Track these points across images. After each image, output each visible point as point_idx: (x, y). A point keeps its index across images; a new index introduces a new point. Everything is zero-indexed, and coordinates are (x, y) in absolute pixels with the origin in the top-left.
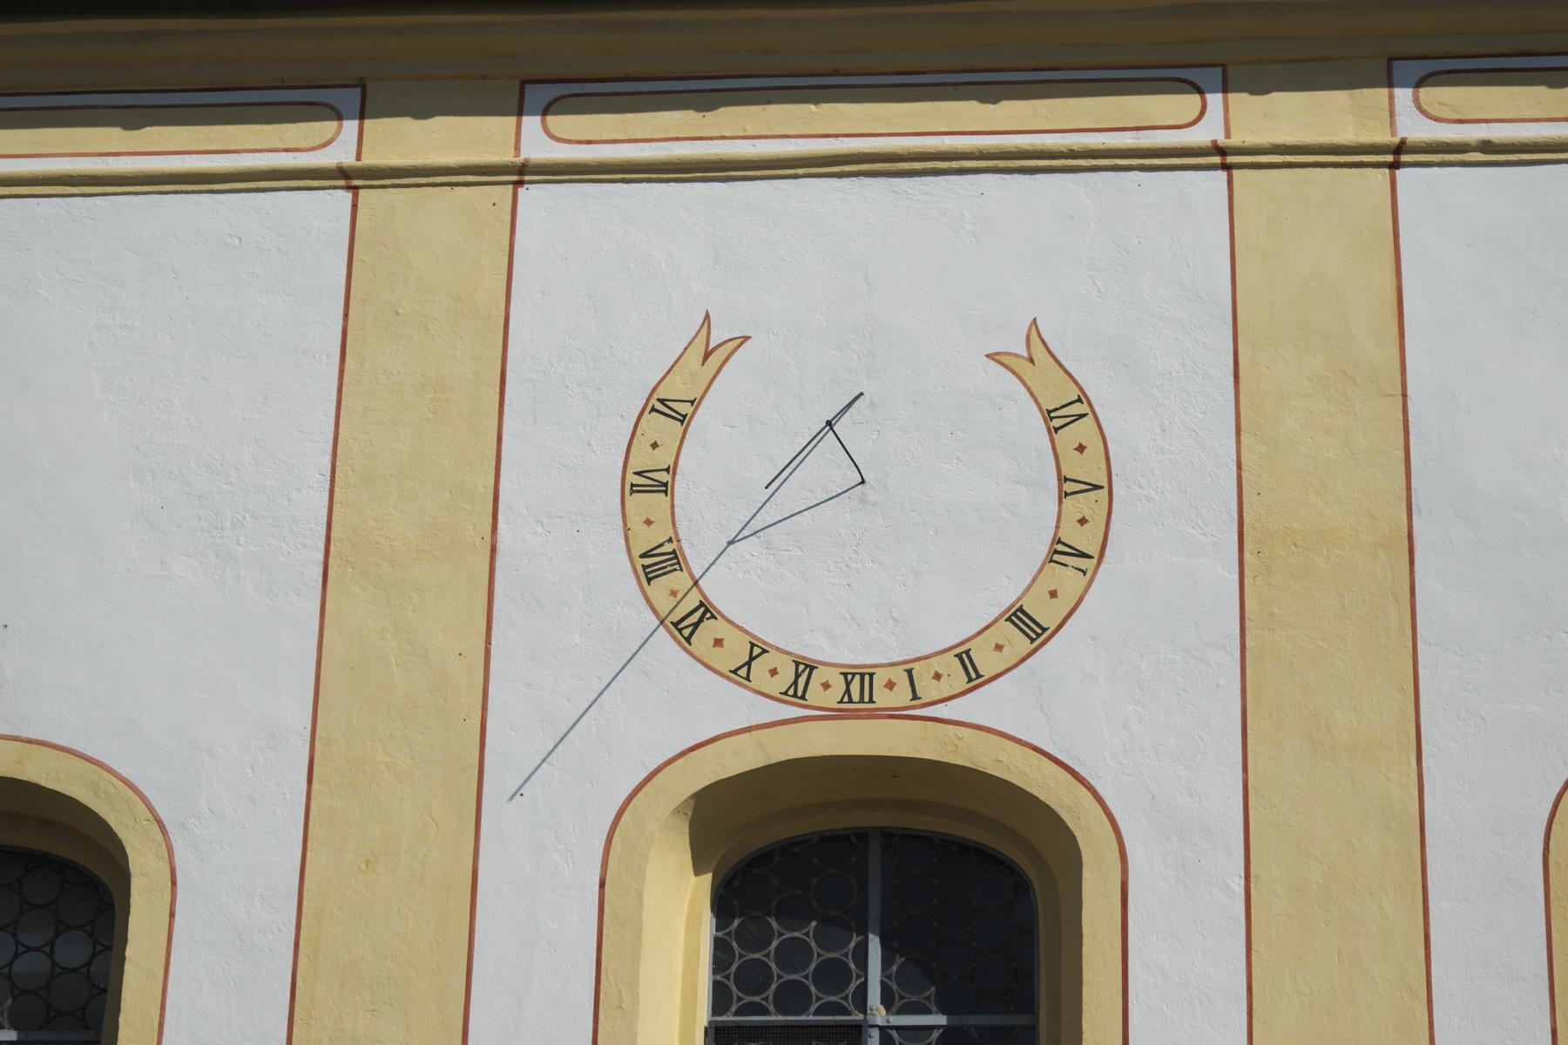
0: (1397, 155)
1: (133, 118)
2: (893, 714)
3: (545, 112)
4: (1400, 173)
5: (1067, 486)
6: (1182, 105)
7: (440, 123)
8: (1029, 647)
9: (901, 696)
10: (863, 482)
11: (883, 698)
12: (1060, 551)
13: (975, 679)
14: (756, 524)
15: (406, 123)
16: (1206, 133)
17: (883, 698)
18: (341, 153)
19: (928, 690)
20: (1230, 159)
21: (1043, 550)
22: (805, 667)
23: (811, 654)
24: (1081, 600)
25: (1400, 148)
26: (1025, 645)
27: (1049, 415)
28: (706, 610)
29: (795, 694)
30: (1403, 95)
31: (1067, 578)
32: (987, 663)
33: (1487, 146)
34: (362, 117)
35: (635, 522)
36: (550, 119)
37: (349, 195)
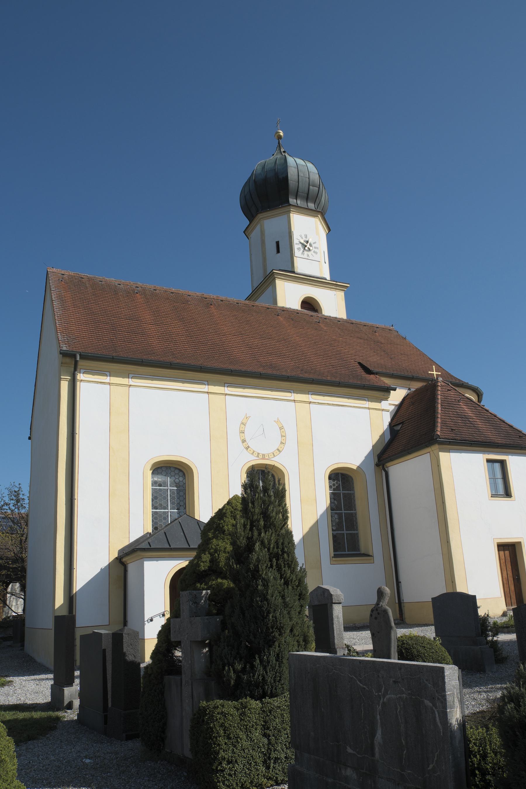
0: (310, 403)
1: (183, 382)
2: (267, 459)
3: (227, 387)
4: (81, 383)
5: (282, 436)
6: (289, 394)
7: (216, 387)
8: (279, 453)
9: (267, 457)
10: (430, 452)
11: (266, 458)
12: (282, 443)
13: (274, 456)
14: (253, 437)
15: (121, 379)
16: (292, 398)
17: (266, 458)
18: (206, 390)
19: (270, 457)
20: (110, 384)
21: (280, 443)
22: (258, 454)
23: (259, 452)
24: (32, 418)
25: (310, 402)
26: (279, 453)
27: (280, 428)
28: (249, 447)
29: (258, 456)
30: (226, 388)
31: (282, 445)
32: (275, 454)
33: (318, 403)
34: (110, 376)
35: (241, 437)
36: (84, 374)
37: (208, 395)
